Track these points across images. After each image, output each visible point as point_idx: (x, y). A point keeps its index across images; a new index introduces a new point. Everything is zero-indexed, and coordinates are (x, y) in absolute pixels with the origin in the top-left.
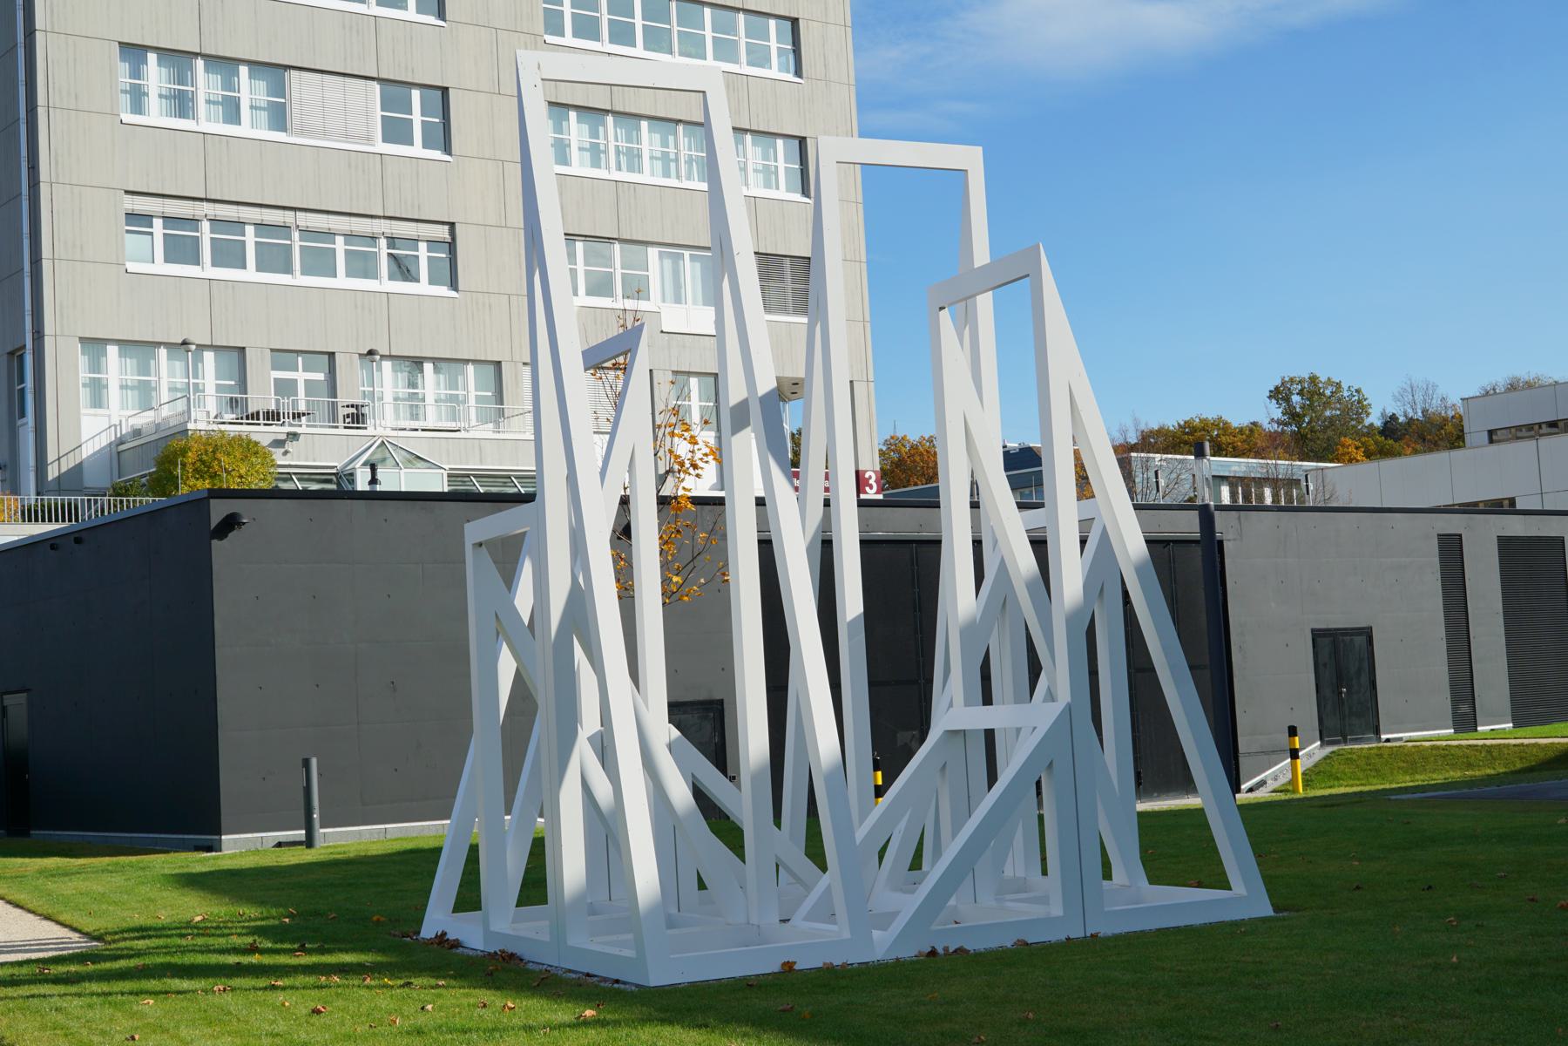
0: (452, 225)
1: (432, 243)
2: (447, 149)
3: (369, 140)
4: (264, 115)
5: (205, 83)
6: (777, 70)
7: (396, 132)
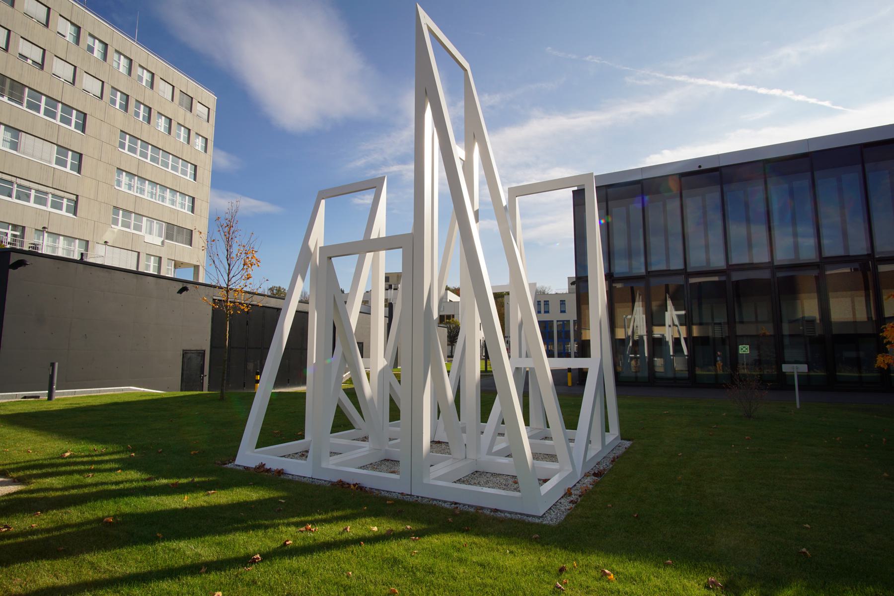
0: (77, 196)
1: (69, 199)
3: (50, 162)
4: (8, 144)
5: (168, 194)
6: (189, 178)
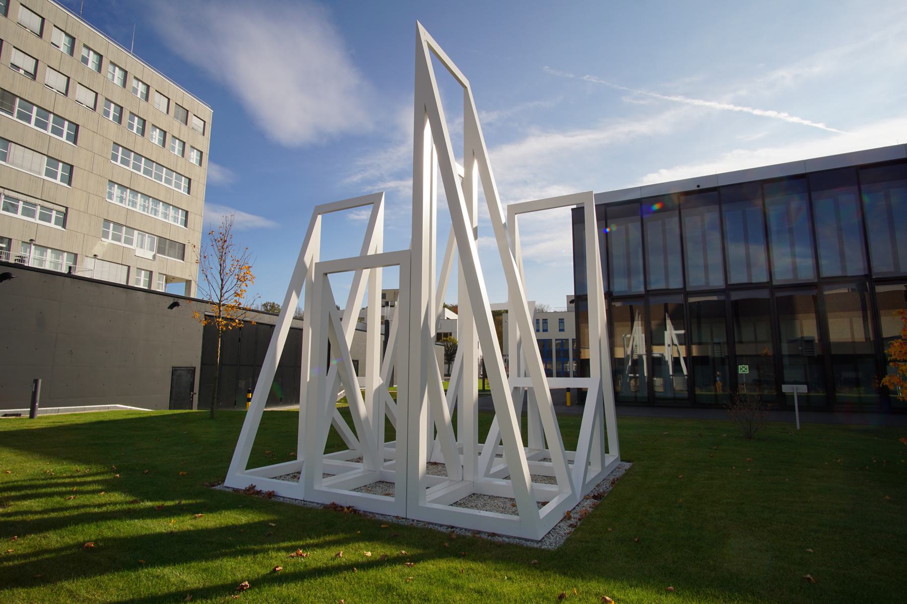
0: (67, 208)
2: (70, 184)
7: (51, 174)
